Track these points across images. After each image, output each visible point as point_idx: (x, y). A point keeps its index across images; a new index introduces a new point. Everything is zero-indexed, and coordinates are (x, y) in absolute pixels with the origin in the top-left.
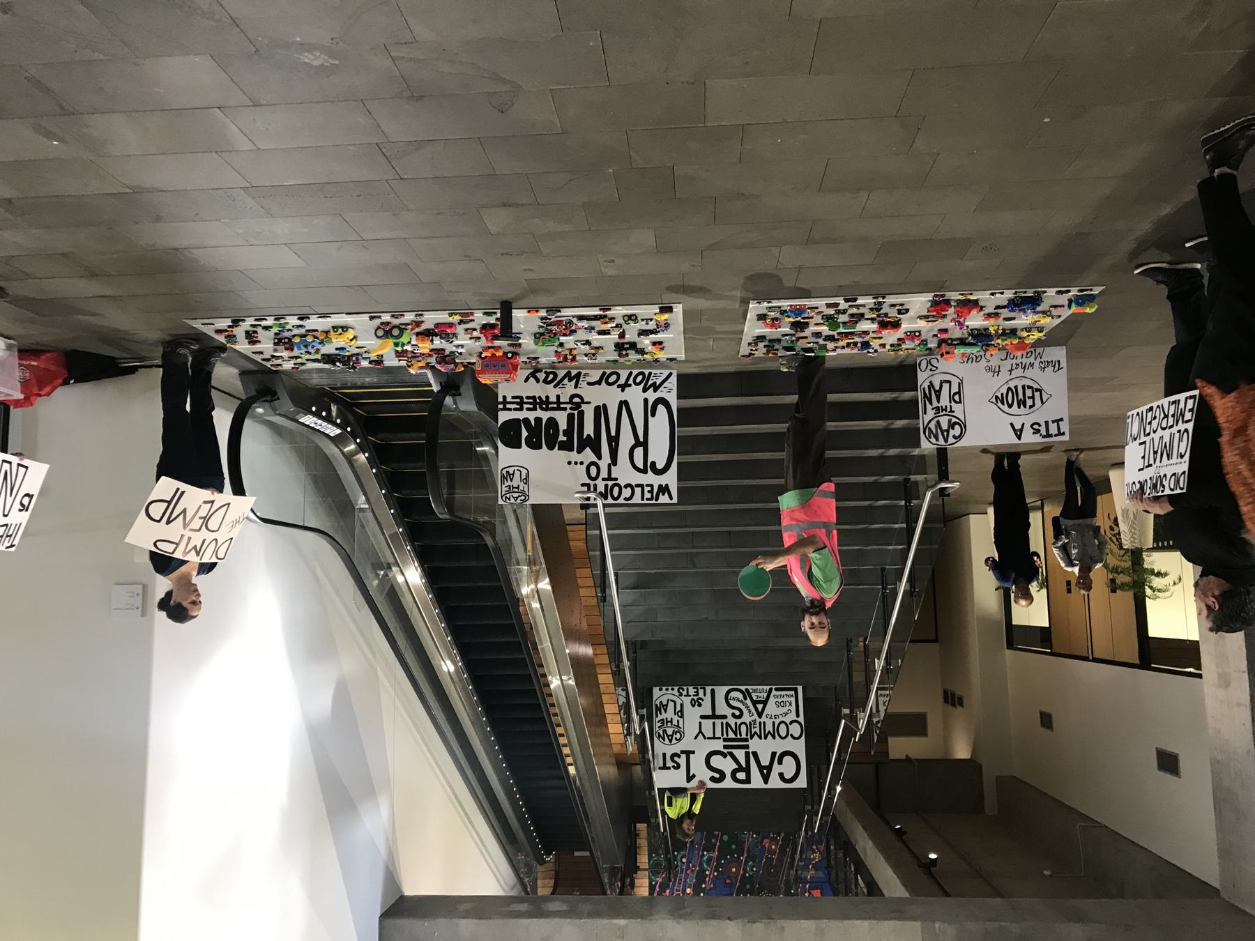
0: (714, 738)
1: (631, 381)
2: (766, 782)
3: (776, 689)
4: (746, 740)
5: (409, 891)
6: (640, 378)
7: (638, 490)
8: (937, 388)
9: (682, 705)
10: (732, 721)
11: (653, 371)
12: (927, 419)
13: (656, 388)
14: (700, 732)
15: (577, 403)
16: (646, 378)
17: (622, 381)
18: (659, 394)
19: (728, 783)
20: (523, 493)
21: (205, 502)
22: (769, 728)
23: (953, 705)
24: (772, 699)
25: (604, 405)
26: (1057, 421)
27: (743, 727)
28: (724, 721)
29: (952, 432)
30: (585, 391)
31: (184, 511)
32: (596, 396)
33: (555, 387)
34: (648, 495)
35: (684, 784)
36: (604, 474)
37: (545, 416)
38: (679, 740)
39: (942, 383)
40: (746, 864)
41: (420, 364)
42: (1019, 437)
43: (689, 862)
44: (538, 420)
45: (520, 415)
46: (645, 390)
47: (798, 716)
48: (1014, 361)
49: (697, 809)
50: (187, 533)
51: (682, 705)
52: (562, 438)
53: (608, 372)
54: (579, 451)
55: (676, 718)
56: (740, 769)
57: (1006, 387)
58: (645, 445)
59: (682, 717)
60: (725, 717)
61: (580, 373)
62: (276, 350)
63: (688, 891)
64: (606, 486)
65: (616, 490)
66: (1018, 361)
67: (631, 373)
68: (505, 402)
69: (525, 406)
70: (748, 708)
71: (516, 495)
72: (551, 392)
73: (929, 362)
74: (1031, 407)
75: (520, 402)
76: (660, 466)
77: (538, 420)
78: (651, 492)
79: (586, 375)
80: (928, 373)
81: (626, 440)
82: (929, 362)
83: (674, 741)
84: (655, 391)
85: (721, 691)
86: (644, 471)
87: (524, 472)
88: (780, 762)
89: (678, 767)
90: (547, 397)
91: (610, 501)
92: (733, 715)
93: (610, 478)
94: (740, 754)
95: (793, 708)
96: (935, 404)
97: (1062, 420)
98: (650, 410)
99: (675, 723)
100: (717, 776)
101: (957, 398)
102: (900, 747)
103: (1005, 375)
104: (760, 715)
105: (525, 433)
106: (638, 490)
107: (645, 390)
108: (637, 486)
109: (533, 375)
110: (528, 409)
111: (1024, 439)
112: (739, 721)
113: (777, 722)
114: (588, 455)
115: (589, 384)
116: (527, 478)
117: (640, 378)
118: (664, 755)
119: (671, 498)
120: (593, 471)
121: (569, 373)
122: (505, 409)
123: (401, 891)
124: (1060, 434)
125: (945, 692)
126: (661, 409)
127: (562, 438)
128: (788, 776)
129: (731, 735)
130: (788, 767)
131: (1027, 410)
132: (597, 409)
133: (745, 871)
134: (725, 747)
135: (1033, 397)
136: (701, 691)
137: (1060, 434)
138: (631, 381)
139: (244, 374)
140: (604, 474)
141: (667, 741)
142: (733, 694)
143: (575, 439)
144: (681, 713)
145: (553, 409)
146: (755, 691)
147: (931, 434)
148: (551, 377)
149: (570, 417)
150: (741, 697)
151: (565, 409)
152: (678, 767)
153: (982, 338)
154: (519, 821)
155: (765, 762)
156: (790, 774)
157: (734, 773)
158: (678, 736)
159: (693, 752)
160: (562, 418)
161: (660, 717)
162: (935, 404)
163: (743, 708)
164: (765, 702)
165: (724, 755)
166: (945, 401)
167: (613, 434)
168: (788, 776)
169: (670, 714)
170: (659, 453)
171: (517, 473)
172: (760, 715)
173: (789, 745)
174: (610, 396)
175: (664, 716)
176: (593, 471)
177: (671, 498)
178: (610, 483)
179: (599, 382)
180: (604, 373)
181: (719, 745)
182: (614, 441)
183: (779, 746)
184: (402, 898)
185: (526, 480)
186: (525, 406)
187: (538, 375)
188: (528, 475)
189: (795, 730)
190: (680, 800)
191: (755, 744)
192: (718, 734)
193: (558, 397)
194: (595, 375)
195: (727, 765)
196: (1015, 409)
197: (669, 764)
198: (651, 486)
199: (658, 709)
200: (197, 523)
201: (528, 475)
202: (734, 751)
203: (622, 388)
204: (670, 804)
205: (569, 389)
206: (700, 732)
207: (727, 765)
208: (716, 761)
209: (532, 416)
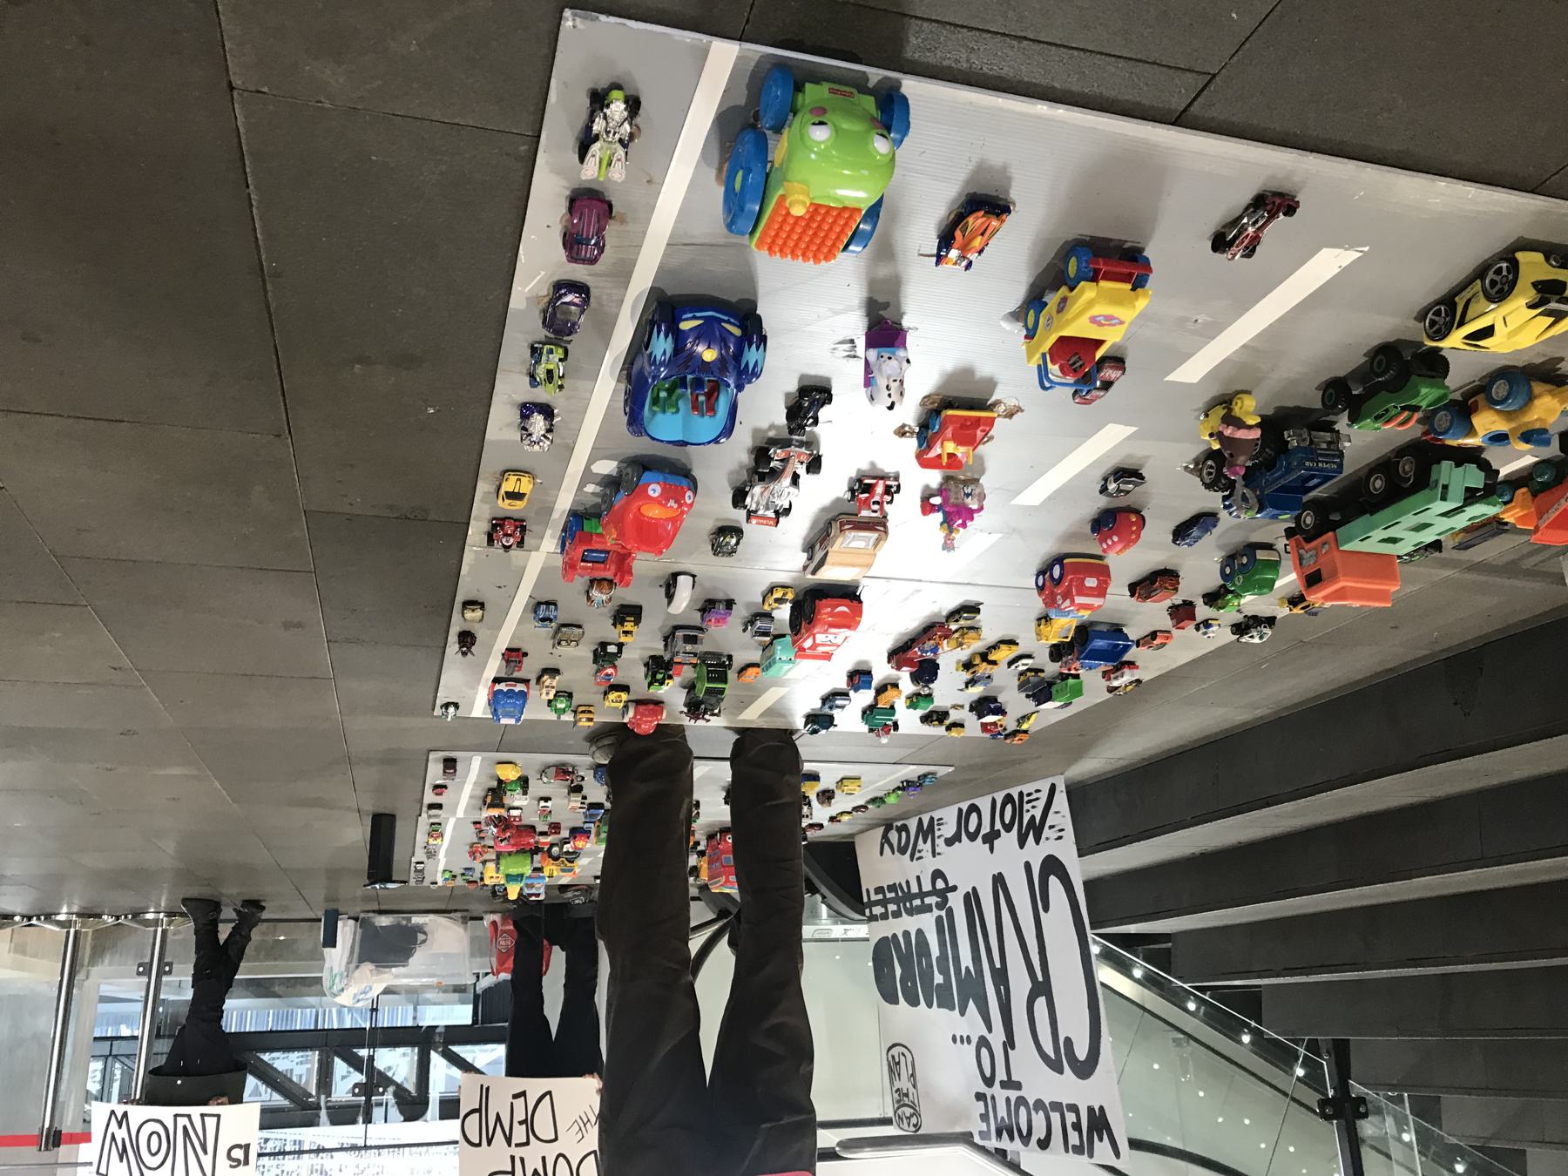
1: (998, 826)
17: (986, 829)
21: (516, 1096)
25: (974, 889)
31: (498, 1118)
50: (519, 1153)
67: (994, 802)
138: (998, 826)
149: (939, 920)
151: (928, 909)
153: (882, 478)
167: (998, 965)
179: (956, 838)
182: (1001, 976)
198: (1074, 1108)
200: (519, 1134)
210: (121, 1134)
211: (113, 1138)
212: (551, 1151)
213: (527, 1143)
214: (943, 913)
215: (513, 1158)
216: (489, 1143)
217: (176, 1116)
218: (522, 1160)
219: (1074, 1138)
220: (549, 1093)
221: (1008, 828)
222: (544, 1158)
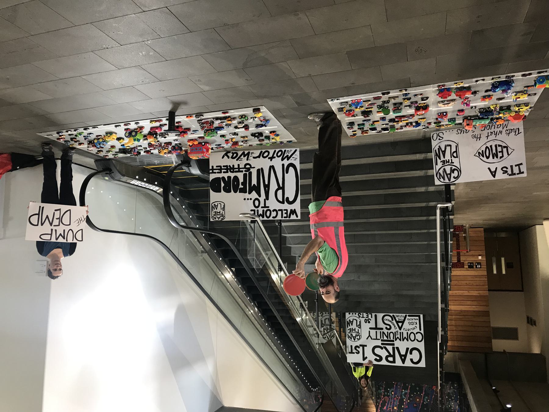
0: (376, 339)
1: (275, 155)
2: (403, 363)
3: (409, 316)
4: (393, 341)
5: (227, 404)
6: (280, 153)
7: (280, 213)
8: (443, 149)
9: (360, 322)
10: (386, 331)
11: (287, 149)
12: (438, 167)
13: (288, 158)
14: (369, 336)
15: (248, 168)
16: (283, 153)
17: (271, 155)
18: (290, 161)
19: (384, 362)
20: (222, 215)
21: (56, 210)
22: (405, 335)
23: (532, 325)
24: (406, 321)
25: (262, 169)
26: (518, 165)
27: (392, 335)
28: (382, 331)
29: (453, 175)
30: (252, 161)
31: (47, 217)
32: (258, 163)
33: (237, 160)
34: (285, 215)
35: (362, 362)
36: (262, 204)
37: (232, 175)
38: (359, 339)
39: (446, 147)
40: (424, 398)
41: (165, 151)
42: (494, 176)
43: (395, 394)
44: (229, 177)
46: (282, 160)
47: (420, 329)
48: (489, 131)
49: (369, 374)
50: (54, 228)
51: (360, 322)
53: (263, 151)
54: (250, 193)
55: (357, 328)
56: (390, 355)
57: (485, 146)
60: (382, 329)
61: (249, 153)
62: (88, 147)
63: (395, 408)
64: (263, 210)
65: (268, 213)
66: (492, 131)
67: (275, 151)
68: (213, 169)
69: (223, 171)
70: (394, 324)
71: (219, 216)
72: (234, 163)
73: (438, 135)
74: (501, 157)
75: (220, 169)
76: (291, 199)
77: (229, 177)
78: (286, 213)
79: (252, 153)
80: (438, 141)
81: (273, 186)
82: (438, 135)
83: (356, 340)
84: (288, 160)
85: (380, 316)
88: (411, 353)
89: (358, 353)
90: (233, 166)
91: (265, 218)
92: (386, 328)
93: (265, 207)
94: (390, 348)
95: (418, 326)
96: (442, 159)
97: (521, 164)
98: (285, 170)
99: (357, 331)
100: (378, 358)
101: (455, 155)
102: (500, 345)
103: (484, 140)
104: (400, 328)
105: (223, 185)
106: (280, 213)
107: (282, 160)
108: (279, 210)
109: (226, 154)
110: (224, 172)
111: (497, 177)
112: (389, 331)
113: (409, 333)
114: (254, 195)
115: (254, 158)
117: (280, 153)
118: (351, 346)
119: (297, 217)
120: (257, 203)
121: (244, 153)
122: (213, 172)
123: (221, 403)
124: (521, 173)
125: (528, 318)
126: (291, 169)
127: (241, 186)
128: (415, 360)
129: (385, 338)
130: (415, 356)
131: (499, 160)
132: (258, 170)
133: (424, 401)
134: (382, 344)
135: (502, 152)
136: (370, 316)
137: (521, 173)
138: (275, 155)
139: (96, 161)
140: (262, 204)
142: (386, 317)
143: (247, 187)
144: (359, 326)
145: (236, 172)
146: (398, 316)
147: (440, 176)
148: (235, 155)
149: (245, 175)
150: (390, 319)
151: (242, 171)
152: (358, 353)
154: (295, 373)
155: (403, 353)
156: (416, 359)
157: (387, 358)
158: (358, 337)
159: (366, 346)
160: (240, 176)
161: (349, 328)
162: (442, 159)
164: (403, 322)
165: (382, 348)
166: (448, 157)
167: (267, 183)
168: (415, 360)
169: (354, 326)
170: (290, 192)
171: (219, 205)
172: (400, 328)
173: (416, 344)
174: (264, 164)
175: (351, 327)
176: (257, 203)
177: (297, 217)
178: (265, 209)
179: (259, 157)
180: (262, 152)
181: (379, 343)
182: (267, 187)
183: (411, 345)
184: (223, 408)
185: (224, 209)
186: (223, 171)
187: (228, 154)
188: (224, 206)
189: (419, 337)
190: (360, 369)
191: (397, 343)
192: (379, 337)
193: (239, 165)
194: (257, 153)
195: (383, 353)
196: (491, 159)
197: (354, 351)
198: (287, 210)
199: (348, 324)
200: (56, 222)
201: (224, 206)
202: (387, 346)
204: (355, 371)
205: (244, 161)
206: (369, 336)
207: (383, 353)
208: (377, 351)
209: (226, 176)
212: (67, 228)
213: (59, 225)
214: (248, 173)
215: (52, 230)
216: (42, 224)
218: (56, 230)
220: (70, 210)
221: (279, 157)
222: (64, 230)
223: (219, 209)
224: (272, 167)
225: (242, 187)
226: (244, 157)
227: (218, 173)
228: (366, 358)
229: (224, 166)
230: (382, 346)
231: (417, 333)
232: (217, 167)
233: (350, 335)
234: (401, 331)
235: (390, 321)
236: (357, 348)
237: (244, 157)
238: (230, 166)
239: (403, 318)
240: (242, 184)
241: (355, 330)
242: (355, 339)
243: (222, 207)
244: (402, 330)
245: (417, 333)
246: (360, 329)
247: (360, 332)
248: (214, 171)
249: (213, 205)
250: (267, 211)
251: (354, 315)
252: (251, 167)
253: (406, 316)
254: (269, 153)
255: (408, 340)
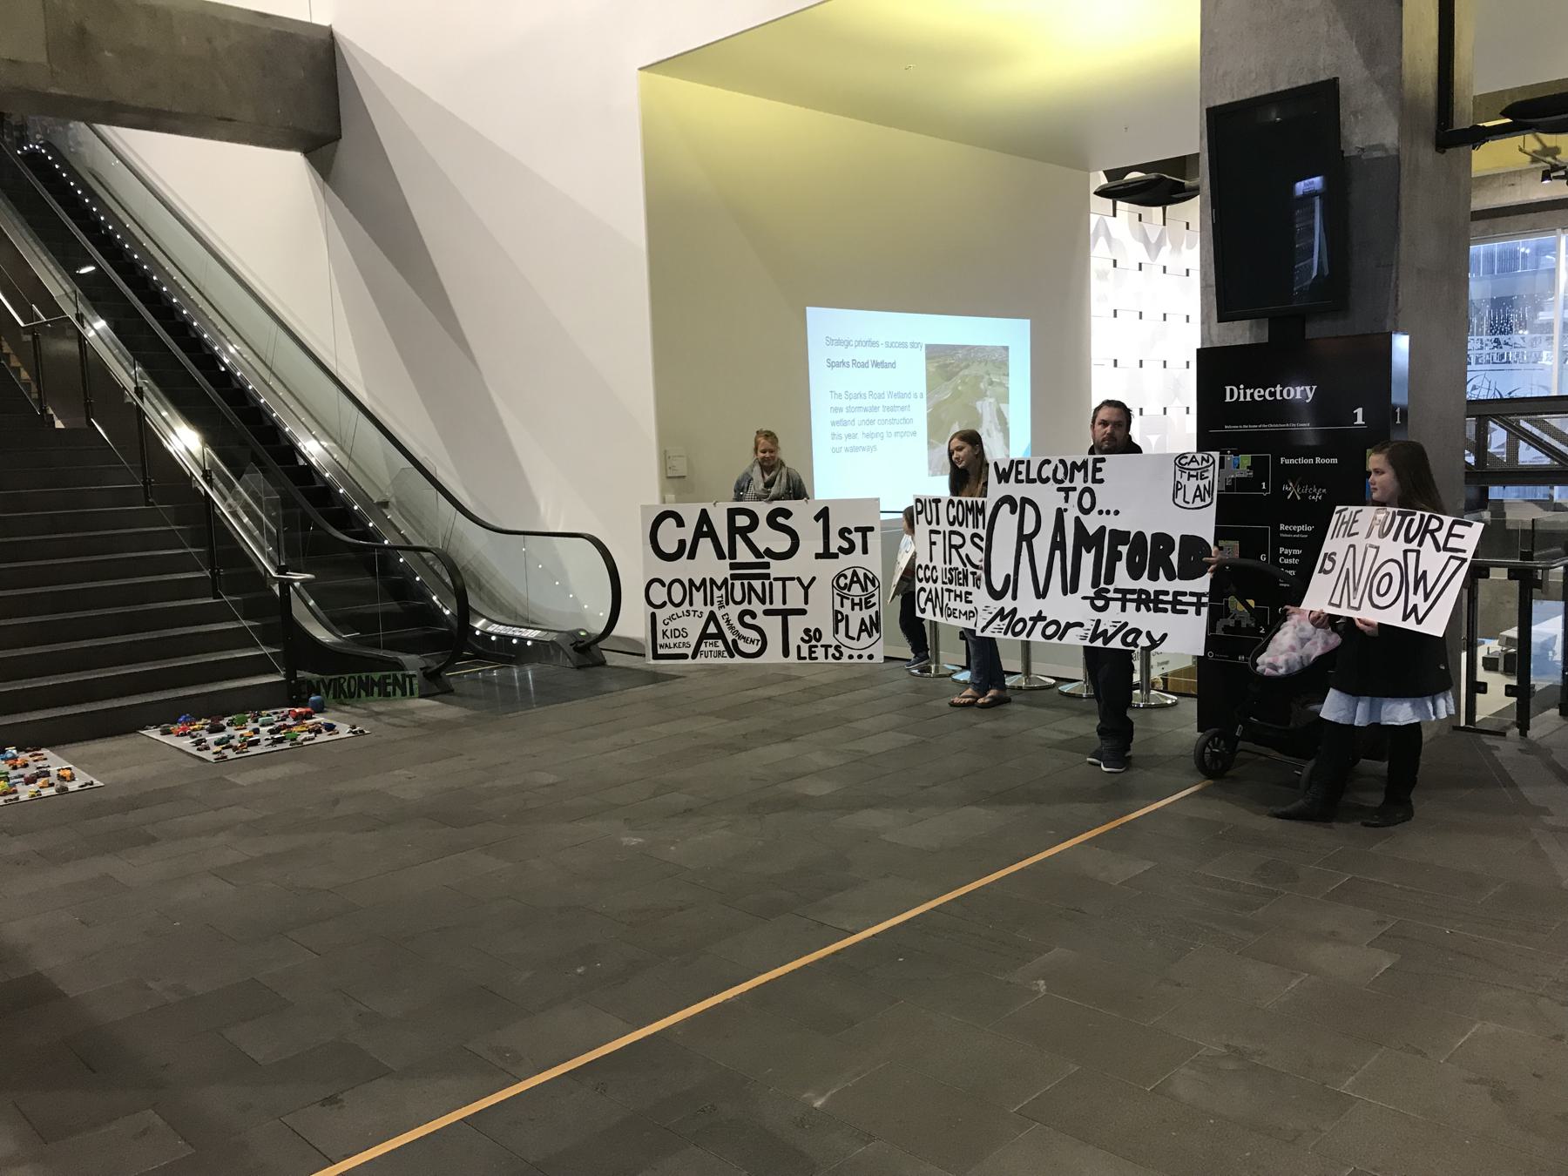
0: (784, 580)
1: (1030, 623)
3: (685, 656)
4: (734, 577)
6: (1018, 628)
7: (1033, 475)
9: (836, 631)
10: (756, 606)
13: (1001, 614)
14: (806, 589)
15: (1100, 600)
17: (1040, 625)
18: (998, 604)
20: (1182, 468)
22: (698, 597)
25: (1065, 593)
27: (738, 597)
28: (768, 606)
30: (1087, 614)
33: (1126, 624)
37: (1144, 583)
38: (842, 575)
44: (1154, 577)
45: (1178, 585)
46: (1014, 611)
51: (836, 631)
52: (1124, 549)
53: (1055, 640)
54: (1103, 529)
55: (847, 610)
56: (744, 532)
58: (1022, 537)
59: (837, 612)
60: (767, 613)
61: (1092, 641)
64: (1071, 480)
69: (1170, 598)
70: (731, 627)
75: (1177, 605)
76: (1006, 508)
77: (1154, 577)
79: (1084, 638)
81: (1042, 543)
83: (849, 573)
84: (1002, 609)
86: (1025, 501)
87: (1179, 500)
88: (682, 543)
89: (843, 532)
90: (1138, 609)
92: (754, 616)
93: (1067, 490)
94: (744, 555)
95: (660, 627)
98: (1011, 583)
99: (847, 603)
100: (780, 520)
104: (712, 617)
105: (1174, 557)
106: (1033, 475)
107: (1014, 611)
108: (1033, 481)
110: (1166, 593)
112: (745, 606)
114: (1092, 524)
115: (1081, 625)
116: (1176, 490)
117: (1018, 628)
118: (865, 551)
120: (1087, 503)
121: (1105, 643)
122: (1199, 595)
126: (998, 586)
127: (1124, 549)
128: (671, 522)
129: (757, 584)
132: (1074, 589)
134: (767, 565)
138: (1030, 623)
140: (1074, 496)
141: (861, 573)
142: (754, 649)
144: (838, 618)
145: (1132, 592)
146: (719, 654)
148: (1129, 639)
149: (1110, 579)
150: (741, 644)
151: (1117, 591)
152: (843, 532)
155: (706, 544)
157: (754, 525)
158: (842, 582)
159: (818, 556)
160: (1122, 578)
161: (872, 611)
163: (738, 627)
164: (704, 636)
165: (769, 552)
167: (1058, 553)
168: (671, 522)
169: (856, 617)
171: (1189, 498)
172: (712, 617)
174: (1061, 606)
176: (1087, 503)
178: (1067, 484)
179: (1069, 626)
180: (1060, 638)
181: (777, 568)
182: (1058, 544)
186: (1170, 598)
187: (1147, 643)
188: (1175, 496)
191: (721, 570)
192: (778, 586)
193: (1123, 609)
195: (765, 537)
197: (857, 538)
198: (1018, 481)
201: (1175, 496)
202: (753, 559)
203: (1040, 617)
206: (806, 589)
207: (765, 537)
208: (782, 543)
209: (1163, 583)
210: (1416, 599)
211: (1426, 597)
214: (1102, 585)
217: (1358, 609)
219: (1022, 468)
223: (1191, 486)
224: (1041, 594)
225: (1120, 548)
226: (1106, 631)
227: (1184, 594)
228: (817, 518)
229: (1165, 611)
230: (767, 559)
231: (664, 604)
232: (1185, 612)
233: (870, 588)
234: (709, 608)
235: (741, 637)
236: (846, 545)
237: (1106, 631)
238: (1148, 609)
239: (703, 648)
240: (1119, 556)
241: (853, 605)
242: (855, 574)
243: (1181, 493)
244: (706, 610)
245: (664, 604)
246: (838, 607)
247: (838, 599)
248: (1194, 600)
249: (1208, 500)
250: (1062, 482)
251: (855, 654)
252: (1092, 599)
253: (694, 657)
254: (1043, 634)
255: (691, 581)
